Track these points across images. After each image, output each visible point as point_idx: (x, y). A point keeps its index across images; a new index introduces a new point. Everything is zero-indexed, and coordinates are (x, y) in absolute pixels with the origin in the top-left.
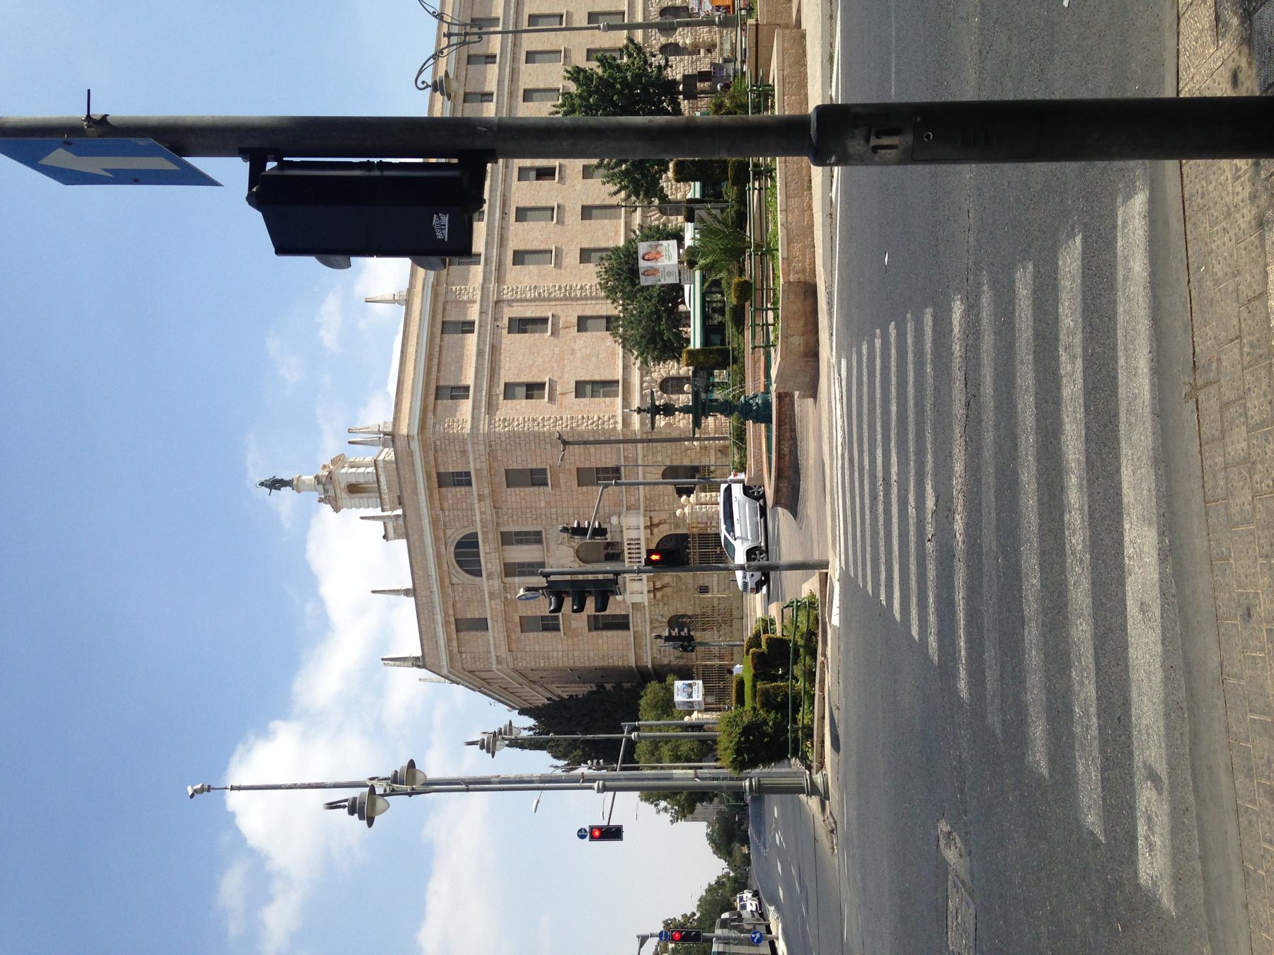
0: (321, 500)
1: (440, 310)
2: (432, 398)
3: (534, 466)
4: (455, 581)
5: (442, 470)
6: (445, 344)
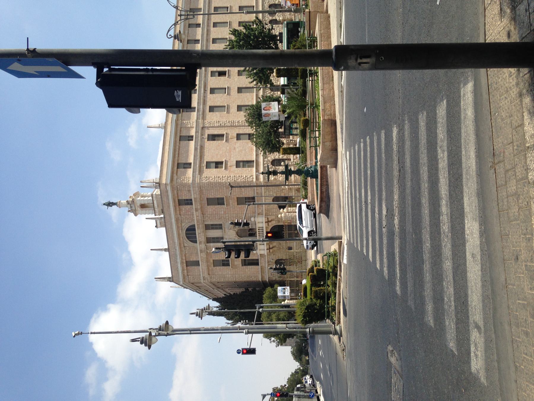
1: (179, 131)
2: (176, 168)
3: (219, 197)
4: (186, 245)
5: (180, 198)
6: (181, 145)
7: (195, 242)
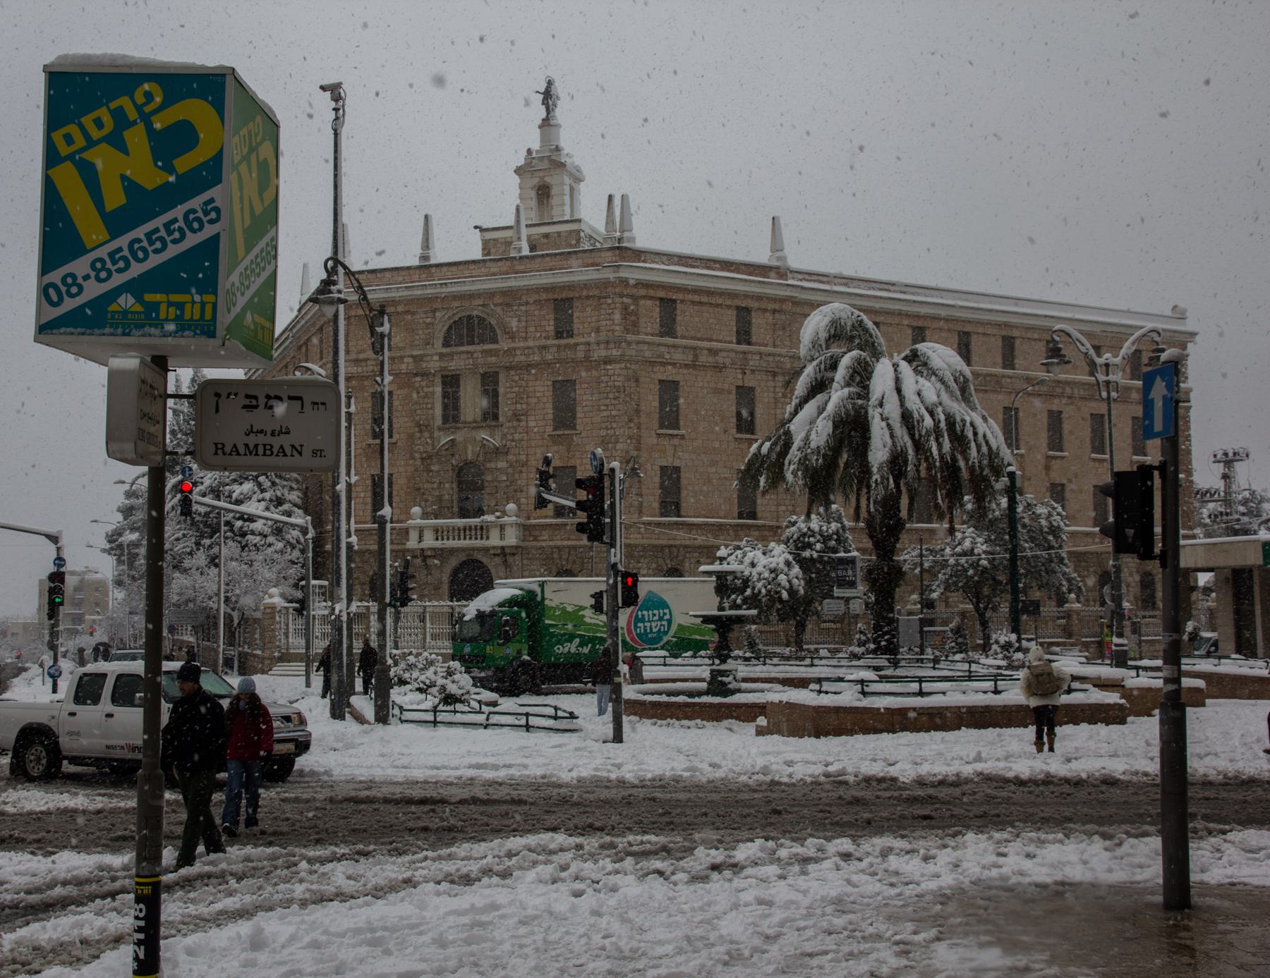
0: (529, 151)
2: (662, 294)
5: (577, 304)
7: (446, 344)
